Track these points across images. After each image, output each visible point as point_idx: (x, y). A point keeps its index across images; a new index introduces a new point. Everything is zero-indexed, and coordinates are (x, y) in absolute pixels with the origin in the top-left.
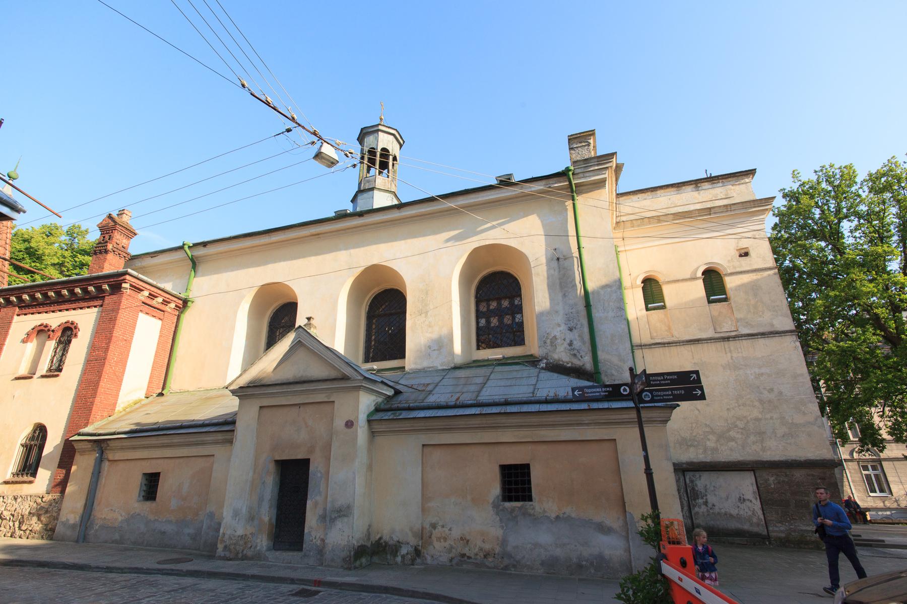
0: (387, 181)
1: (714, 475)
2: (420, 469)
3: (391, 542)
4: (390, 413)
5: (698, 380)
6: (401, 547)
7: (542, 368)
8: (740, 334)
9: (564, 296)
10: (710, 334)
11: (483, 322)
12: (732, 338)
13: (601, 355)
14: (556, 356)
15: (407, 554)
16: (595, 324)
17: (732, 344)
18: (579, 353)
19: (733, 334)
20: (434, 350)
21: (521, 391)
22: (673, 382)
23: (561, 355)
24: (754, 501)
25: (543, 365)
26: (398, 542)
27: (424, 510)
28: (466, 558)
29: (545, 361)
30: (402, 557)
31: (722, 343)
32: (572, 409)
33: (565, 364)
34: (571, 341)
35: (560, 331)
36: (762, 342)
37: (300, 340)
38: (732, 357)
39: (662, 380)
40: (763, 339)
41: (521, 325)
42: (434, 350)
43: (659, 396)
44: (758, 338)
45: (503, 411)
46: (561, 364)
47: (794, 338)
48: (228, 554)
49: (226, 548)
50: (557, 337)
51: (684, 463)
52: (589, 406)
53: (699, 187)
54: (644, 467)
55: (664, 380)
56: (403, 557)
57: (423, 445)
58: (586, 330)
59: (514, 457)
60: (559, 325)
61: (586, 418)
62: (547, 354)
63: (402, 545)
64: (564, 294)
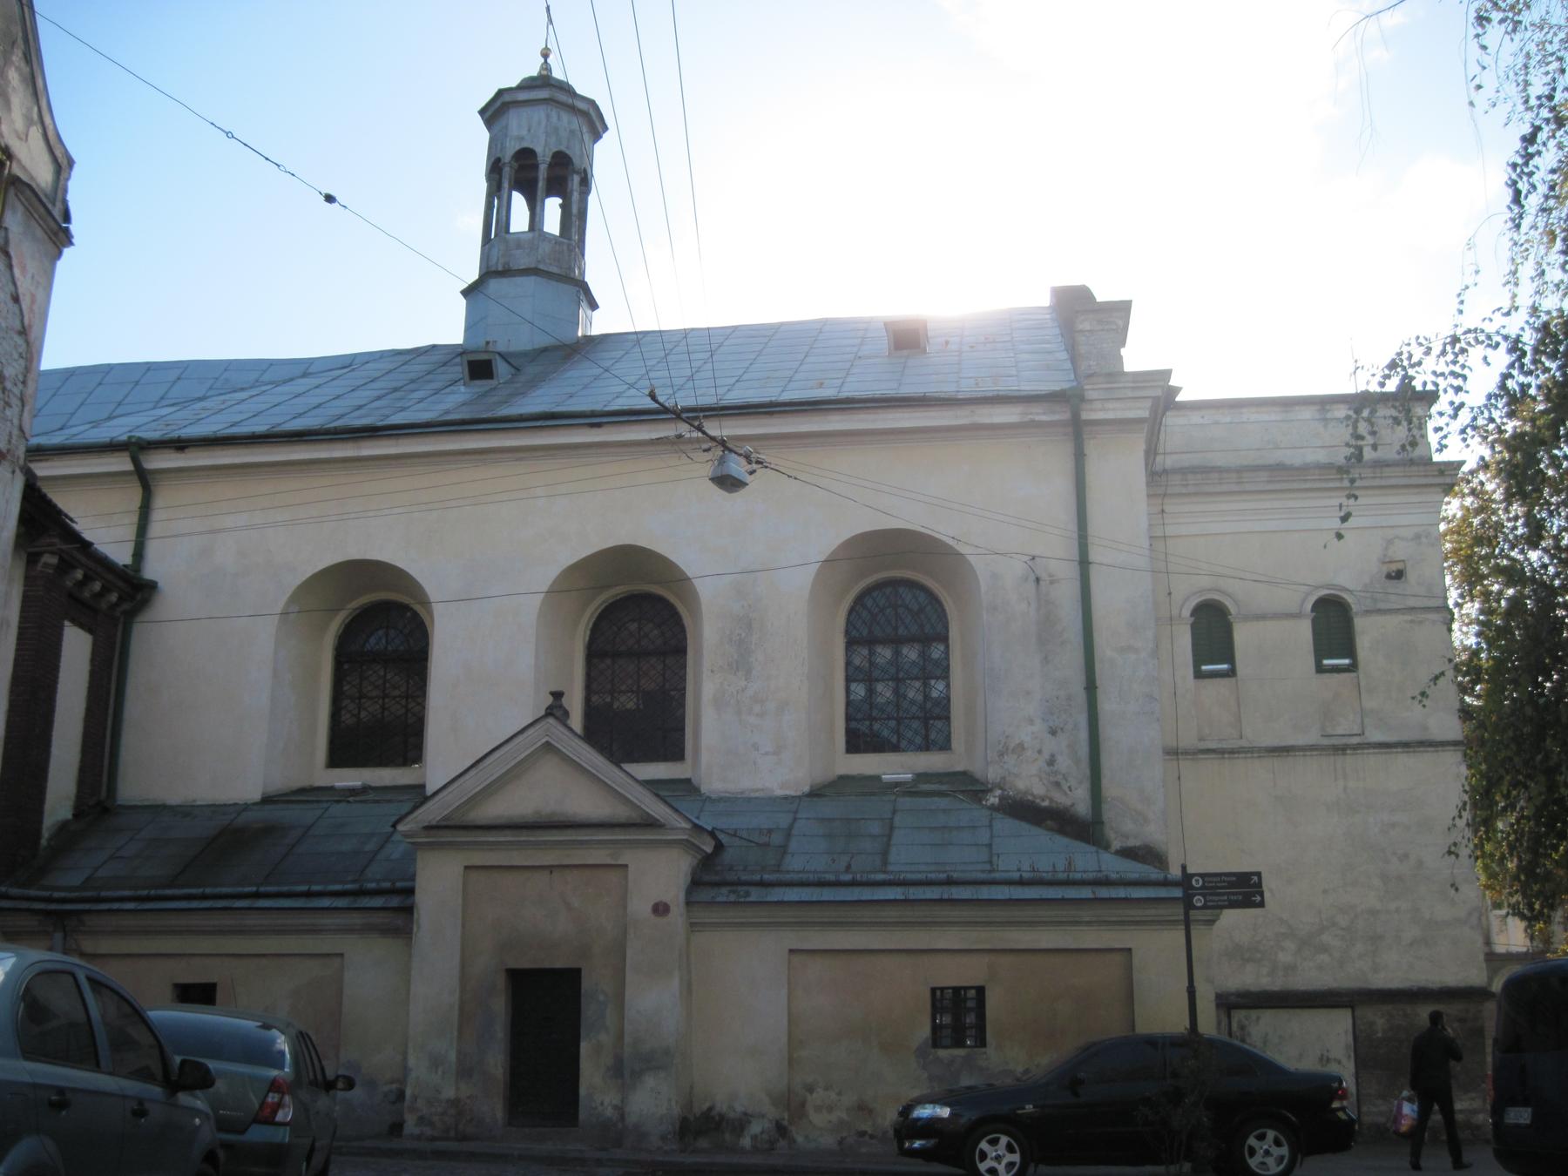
0: (565, 247)
1: (1283, 1014)
2: (784, 992)
3: (732, 1115)
4: (724, 890)
5: (1259, 885)
6: (750, 1122)
7: (993, 808)
8: (1366, 741)
9: (1046, 660)
10: (1313, 737)
11: (859, 690)
12: (1351, 748)
13: (1110, 789)
14: (1021, 785)
15: (762, 1132)
16: (1101, 723)
17: (1349, 760)
18: (1066, 780)
19: (1355, 740)
20: (767, 754)
21: (963, 858)
22: (1231, 885)
23: (1029, 780)
24: (1344, 1061)
25: (993, 799)
26: (745, 1114)
27: (791, 1062)
28: (867, 1138)
29: (998, 792)
30: (752, 1138)
31: (1332, 758)
32: (1066, 896)
33: (1038, 801)
34: (1053, 756)
35: (1033, 733)
36: (1402, 760)
37: (547, 742)
38: (1345, 788)
39: (1219, 882)
40: (1405, 754)
41: (945, 703)
42: (767, 754)
43: (1212, 882)
44: (1397, 752)
45: (946, 896)
46: (1029, 800)
47: (1458, 756)
48: (428, 1131)
49: (422, 1120)
50: (1026, 745)
51: (1232, 994)
52: (1094, 893)
53: (1329, 411)
54: (1186, 984)
55: (1221, 882)
56: (754, 1138)
57: (791, 951)
58: (1083, 735)
59: (954, 974)
60: (1031, 722)
61: (1086, 914)
62: (1003, 778)
63: (752, 1119)
64: (1046, 658)
